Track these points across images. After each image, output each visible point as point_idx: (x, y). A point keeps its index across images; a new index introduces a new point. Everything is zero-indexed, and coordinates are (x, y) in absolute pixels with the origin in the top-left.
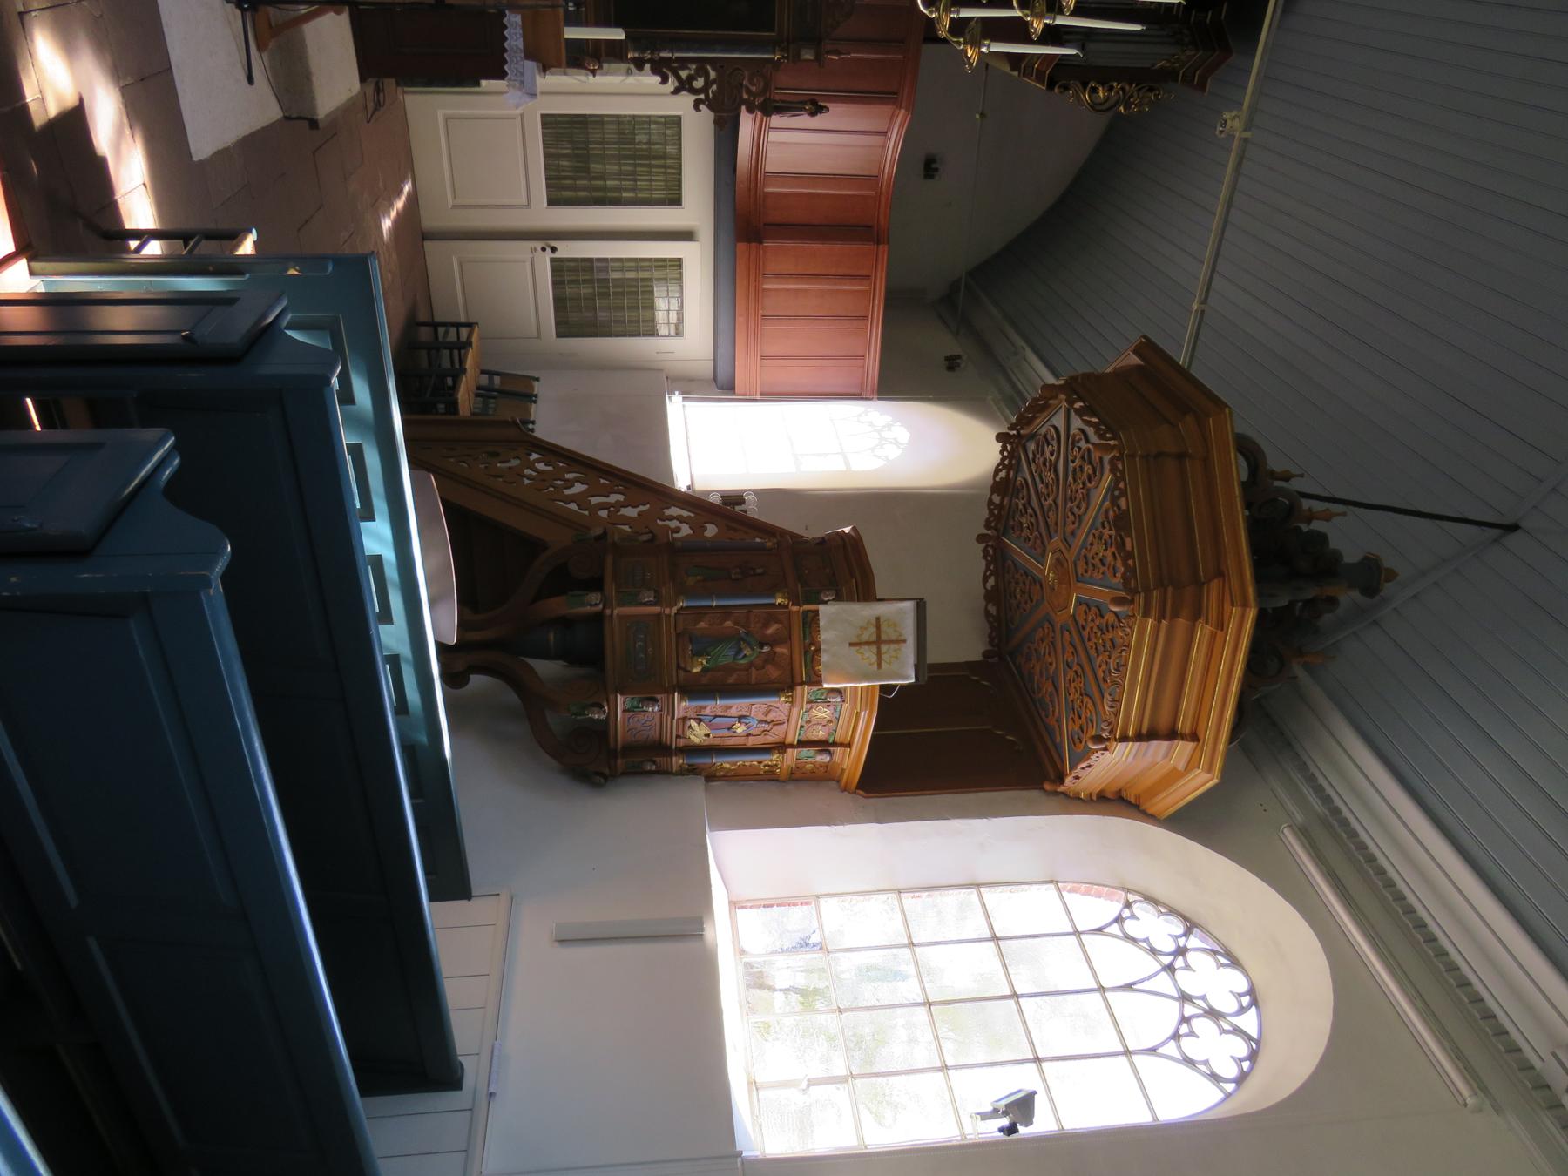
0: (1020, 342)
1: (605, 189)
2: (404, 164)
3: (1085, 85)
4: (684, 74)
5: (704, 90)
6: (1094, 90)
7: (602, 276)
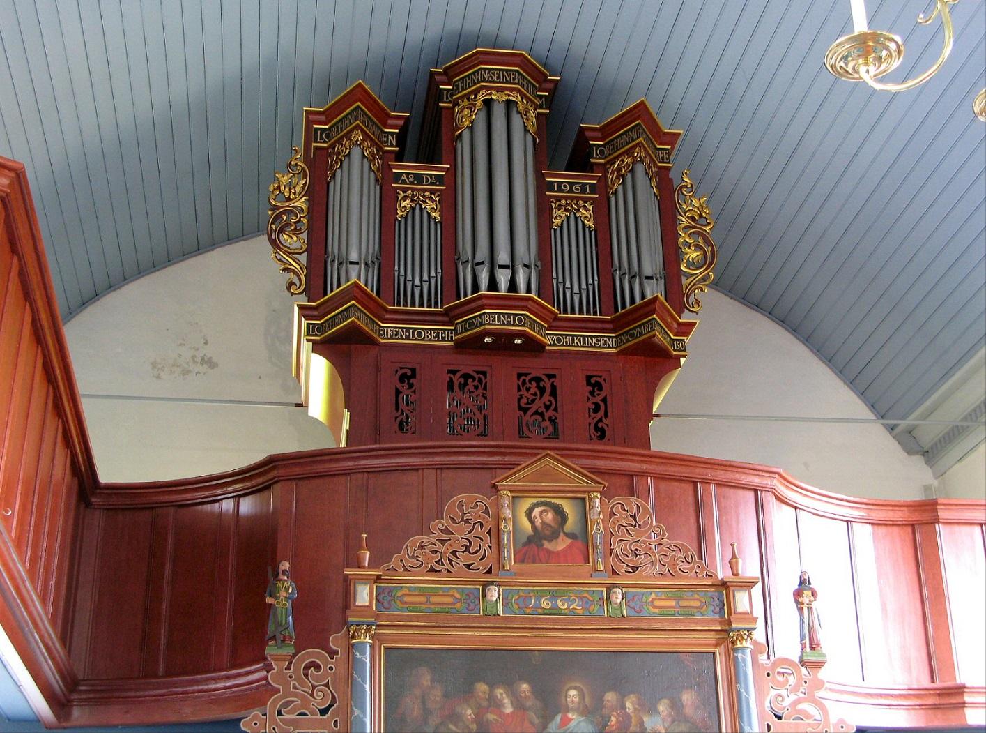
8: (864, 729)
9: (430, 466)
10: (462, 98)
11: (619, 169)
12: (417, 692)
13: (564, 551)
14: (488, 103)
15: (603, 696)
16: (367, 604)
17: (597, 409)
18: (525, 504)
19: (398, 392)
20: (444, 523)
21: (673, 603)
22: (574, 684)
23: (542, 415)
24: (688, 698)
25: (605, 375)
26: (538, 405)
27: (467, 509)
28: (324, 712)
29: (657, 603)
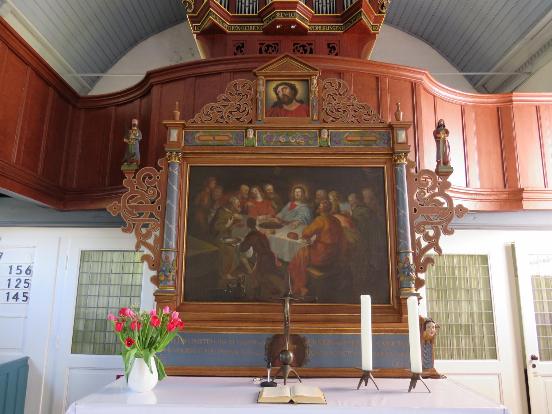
1: (480, 314)
4: (424, 244)
9: (227, 71)
12: (208, 190)
15: (316, 192)
16: (176, 140)
18: (273, 85)
20: (224, 96)
25: (337, 43)
27: (239, 86)
29: (349, 138)
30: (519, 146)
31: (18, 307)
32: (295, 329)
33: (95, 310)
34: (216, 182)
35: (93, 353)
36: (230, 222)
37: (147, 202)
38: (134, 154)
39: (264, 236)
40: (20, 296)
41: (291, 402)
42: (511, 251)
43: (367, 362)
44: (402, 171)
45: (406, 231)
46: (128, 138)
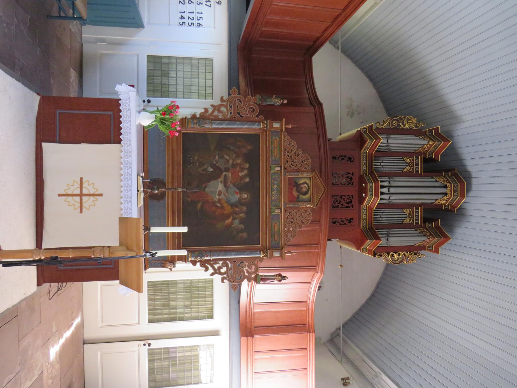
0: (377, 370)
2: (80, 307)
3: (388, 254)
4: (216, 266)
5: (226, 273)
6: (392, 255)
7: (174, 355)
8: (240, 328)
9: (320, 155)
10: (447, 178)
11: (425, 232)
13: (292, 194)
14: (446, 187)
17: (343, 221)
18: (308, 181)
19: (345, 156)
20: (301, 153)
21: (276, 230)
22: (249, 197)
23: (340, 203)
24: (245, 235)
25: (353, 224)
26: (343, 202)
28: (239, 113)
29: (276, 225)
30: (280, 336)
31: (175, 19)
32: (169, 193)
33: (175, 69)
34: (250, 149)
35: (148, 70)
36: (227, 158)
37: (238, 110)
38: (266, 102)
39: (219, 177)
40: (183, 20)
41: (138, 191)
42: (215, 333)
43: (154, 230)
44: (257, 254)
45: (223, 255)
46: (276, 98)
